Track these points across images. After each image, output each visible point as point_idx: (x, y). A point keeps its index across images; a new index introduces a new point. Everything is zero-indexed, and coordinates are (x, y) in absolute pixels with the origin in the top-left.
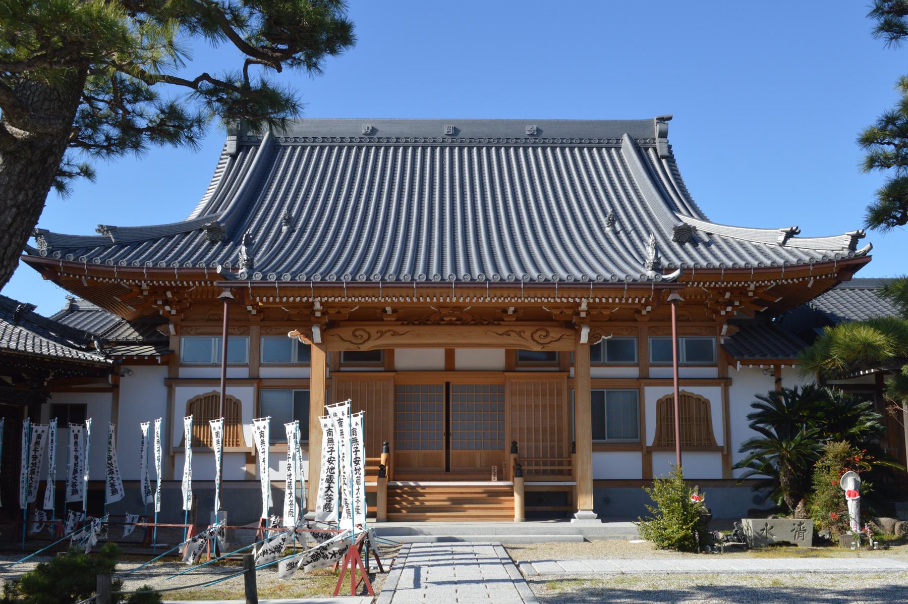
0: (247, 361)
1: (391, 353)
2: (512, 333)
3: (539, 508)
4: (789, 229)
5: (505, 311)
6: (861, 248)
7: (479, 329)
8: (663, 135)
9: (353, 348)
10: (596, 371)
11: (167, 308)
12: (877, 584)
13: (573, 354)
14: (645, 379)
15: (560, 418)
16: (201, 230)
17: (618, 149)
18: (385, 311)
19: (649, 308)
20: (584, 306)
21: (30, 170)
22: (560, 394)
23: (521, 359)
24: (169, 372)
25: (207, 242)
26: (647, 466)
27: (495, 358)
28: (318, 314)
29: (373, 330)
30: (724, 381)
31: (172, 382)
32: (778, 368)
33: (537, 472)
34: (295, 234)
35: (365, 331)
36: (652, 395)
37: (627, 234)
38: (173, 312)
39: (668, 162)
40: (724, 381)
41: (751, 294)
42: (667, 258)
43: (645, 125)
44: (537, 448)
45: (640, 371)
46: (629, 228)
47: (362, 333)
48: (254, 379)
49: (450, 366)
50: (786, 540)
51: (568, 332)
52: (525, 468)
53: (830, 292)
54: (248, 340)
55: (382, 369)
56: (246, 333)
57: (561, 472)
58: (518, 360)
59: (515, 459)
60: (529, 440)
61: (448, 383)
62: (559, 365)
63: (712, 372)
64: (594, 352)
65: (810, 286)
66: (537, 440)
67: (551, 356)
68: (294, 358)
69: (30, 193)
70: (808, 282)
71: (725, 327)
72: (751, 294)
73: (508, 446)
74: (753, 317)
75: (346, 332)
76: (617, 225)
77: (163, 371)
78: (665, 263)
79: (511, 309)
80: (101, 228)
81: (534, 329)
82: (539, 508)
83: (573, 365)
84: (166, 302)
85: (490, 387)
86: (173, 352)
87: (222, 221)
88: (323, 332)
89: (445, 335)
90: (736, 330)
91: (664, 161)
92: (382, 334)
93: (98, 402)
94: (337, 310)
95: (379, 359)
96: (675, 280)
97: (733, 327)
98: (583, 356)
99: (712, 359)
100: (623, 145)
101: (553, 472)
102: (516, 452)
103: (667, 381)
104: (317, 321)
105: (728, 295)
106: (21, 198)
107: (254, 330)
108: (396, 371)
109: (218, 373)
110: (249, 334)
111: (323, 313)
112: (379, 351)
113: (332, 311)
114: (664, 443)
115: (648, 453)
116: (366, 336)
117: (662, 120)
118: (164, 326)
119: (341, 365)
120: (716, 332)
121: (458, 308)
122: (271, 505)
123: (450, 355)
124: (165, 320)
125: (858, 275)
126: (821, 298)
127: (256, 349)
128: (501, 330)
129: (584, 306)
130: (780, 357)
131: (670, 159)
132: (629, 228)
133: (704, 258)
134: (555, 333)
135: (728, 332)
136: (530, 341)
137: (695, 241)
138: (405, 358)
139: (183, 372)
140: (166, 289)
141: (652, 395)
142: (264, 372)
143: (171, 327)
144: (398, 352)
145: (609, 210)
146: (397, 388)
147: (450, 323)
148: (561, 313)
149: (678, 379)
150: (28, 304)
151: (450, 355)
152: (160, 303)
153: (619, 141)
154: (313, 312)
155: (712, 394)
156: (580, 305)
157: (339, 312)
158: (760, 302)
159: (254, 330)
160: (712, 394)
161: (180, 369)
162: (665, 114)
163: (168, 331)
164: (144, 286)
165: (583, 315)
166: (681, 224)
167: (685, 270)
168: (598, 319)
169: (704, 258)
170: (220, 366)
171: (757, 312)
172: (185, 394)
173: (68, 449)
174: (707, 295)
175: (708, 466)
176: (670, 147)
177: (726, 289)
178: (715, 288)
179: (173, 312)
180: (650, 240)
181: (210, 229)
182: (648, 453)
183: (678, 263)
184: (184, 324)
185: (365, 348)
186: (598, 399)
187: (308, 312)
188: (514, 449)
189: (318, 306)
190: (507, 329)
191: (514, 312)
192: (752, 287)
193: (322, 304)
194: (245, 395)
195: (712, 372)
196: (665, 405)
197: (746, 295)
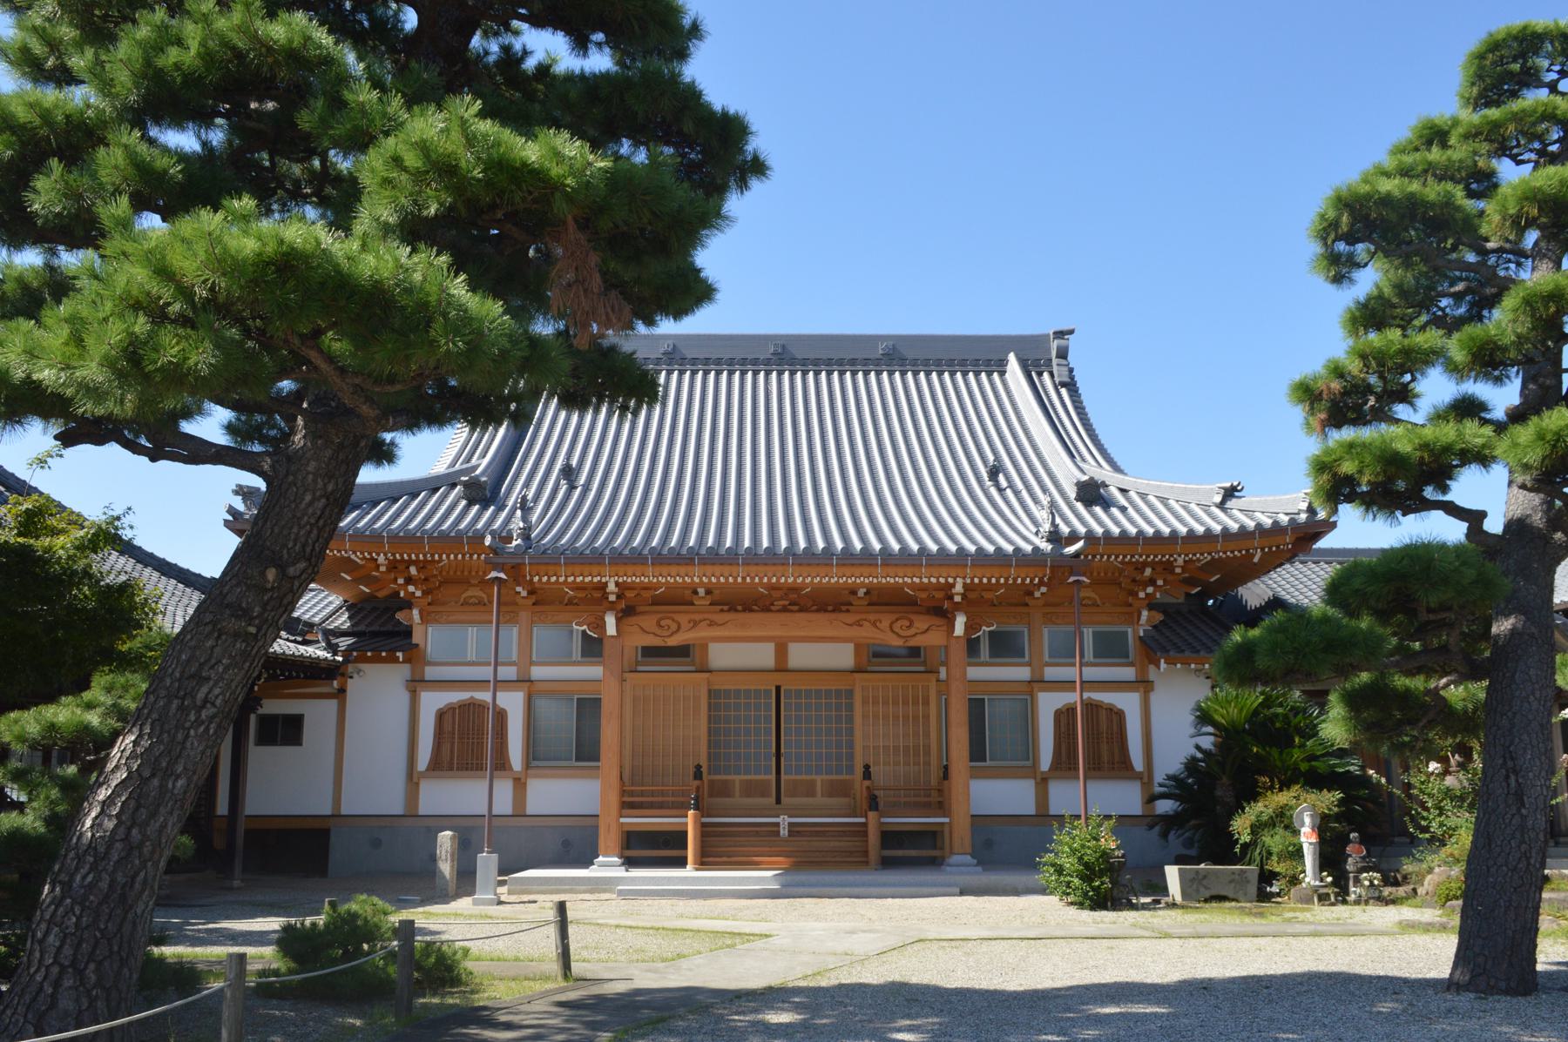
0: (515, 658)
1: (705, 647)
3: (900, 853)
4: (1228, 485)
5: (854, 592)
8: (1063, 354)
9: (657, 642)
10: (975, 673)
11: (411, 588)
12: (1227, 904)
14: (1038, 683)
15: (927, 734)
16: (454, 486)
17: (1002, 373)
18: (695, 592)
19: (1043, 589)
20: (959, 588)
21: (341, 456)
22: (926, 702)
23: (876, 655)
25: (464, 502)
26: (1042, 798)
27: (841, 655)
28: (612, 598)
29: (683, 619)
30: (1143, 685)
31: (416, 684)
34: (577, 492)
36: (1048, 704)
37: (1017, 493)
38: (418, 594)
39: (1069, 391)
40: (1143, 685)
41: (1178, 570)
42: (1067, 522)
43: (1039, 341)
45: (1033, 671)
46: (1020, 485)
48: (524, 681)
49: (781, 667)
50: (1223, 893)
53: (1287, 566)
54: (515, 630)
56: (513, 620)
58: (873, 658)
62: (924, 663)
63: (1128, 673)
64: (972, 646)
65: (1256, 560)
67: (915, 652)
69: (341, 480)
70: (1253, 555)
71: (1145, 613)
72: (1178, 570)
73: (859, 770)
74: (1181, 600)
75: (648, 622)
76: (1001, 478)
78: (1065, 530)
79: (861, 592)
81: (894, 617)
82: (900, 853)
84: (409, 580)
85: (834, 693)
87: (483, 473)
88: (618, 620)
89: (775, 625)
90: (1159, 617)
91: (1064, 391)
92: (695, 624)
93: (317, 714)
96: (1077, 555)
97: (1154, 613)
98: (958, 653)
100: (1009, 368)
103: (1067, 685)
104: (612, 607)
105: (1148, 572)
106: (330, 487)
107: (524, 616)
109: (486, 672)
111: (619, 597)
114: (1064, 763)
115: (1043, 782)
116: (674, 627)
117: (1060, 334)
118: (406, 612)
119: (637, 663)
121: (794, 589)
123: (781, 651)
124: (408, 604)
125: (1323, 543)
126: (1273, 575)
128: (850, 618)
129: (959, 588)
131: (1071, 385)
132: (1020, 485)
133: (1117, 523)
134: (921, 623)
136: (887, 632)
137: (1107, 504)
138: (724, 655)
139: (431, 673)
140: (410, 562)
141: (1048, 704)
142: (538, 672)
143: (415, 612)
144: (714, 649)
145: (991, 457)
146: (712, 694)
147: (784, 610)
149: (1082, 682)
151: (781, 651)
154: (605, 596)
156: (953, 585)
158: (1190, 582)
159: (524, 616)
160: (1128, 702)
162: (1065, 327)
163: (411, 618)
164: (381, 559)
165: (958, 599)
166: (1085, 478)
167: (1090, 537)
168: (976, 602)
169: (1117, 523)
170: (488, 664)
171: (1188, 595)
173: (51, 698)
174: (1121, 571)
175: (1125, 798)
176: (1071, 370)
177: (1145, 564)
178: (1130, 562)
180: (1044, 500)
181: (466, 485)
182: (1043, 782)
183: (1082, 530)
184: (431, 608)
185: (673, 641)
186: (976, 709)
187: (597, 595)
189: (612, 587)
190: (858, 617)
192: (1180, 561)
193: (617, 584)
195: (1128, 673)
196: (1064, 717)
197: (1172, 572)
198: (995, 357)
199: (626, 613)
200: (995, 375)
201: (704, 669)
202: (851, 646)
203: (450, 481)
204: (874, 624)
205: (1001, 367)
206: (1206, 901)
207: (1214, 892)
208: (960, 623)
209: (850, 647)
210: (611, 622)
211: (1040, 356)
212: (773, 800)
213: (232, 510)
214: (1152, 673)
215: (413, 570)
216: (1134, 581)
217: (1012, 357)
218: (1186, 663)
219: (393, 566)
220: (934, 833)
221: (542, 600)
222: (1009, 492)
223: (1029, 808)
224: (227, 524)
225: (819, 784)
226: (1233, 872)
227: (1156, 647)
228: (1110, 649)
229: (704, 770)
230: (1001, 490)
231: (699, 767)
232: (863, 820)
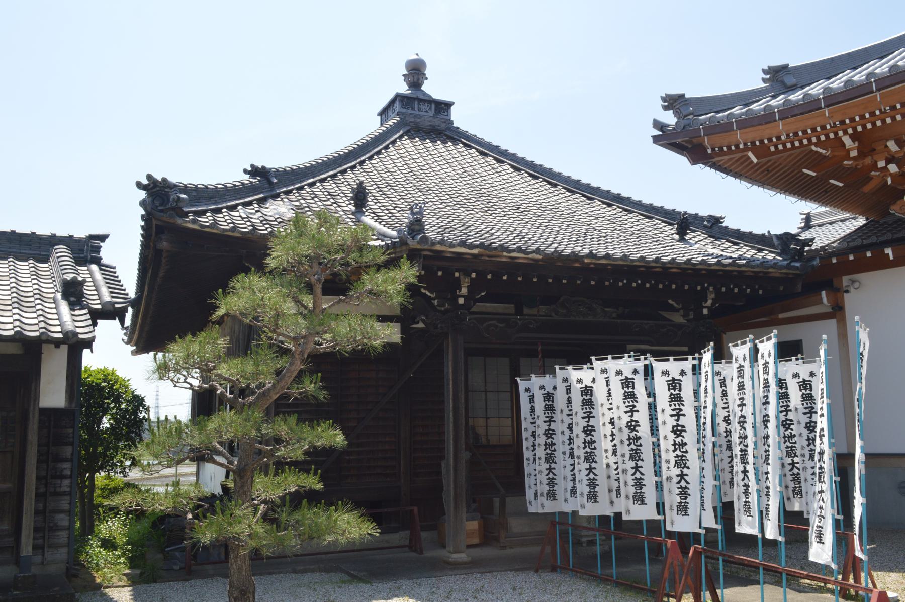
80: (384, 113)
152: (881, 164)
213: (657, 124)
215: (892, 146)
224: (656, 140)
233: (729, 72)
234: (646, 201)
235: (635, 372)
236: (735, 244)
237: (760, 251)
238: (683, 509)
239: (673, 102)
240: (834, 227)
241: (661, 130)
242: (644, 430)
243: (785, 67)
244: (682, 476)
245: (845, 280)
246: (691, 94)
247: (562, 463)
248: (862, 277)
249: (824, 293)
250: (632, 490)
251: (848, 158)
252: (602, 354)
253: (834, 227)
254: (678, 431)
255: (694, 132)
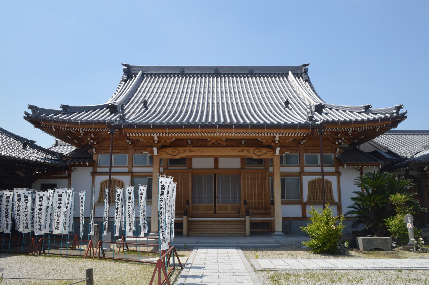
0: (127, 165)
2: (245, 151)
3: (257, 230)
6: (401, 111)
7: (230, 149)
9: (172, 157)
11: (92, 141)
13: (272, 160)
14: (302, 173)
17: (287, 78)
20: (277, 138)
24: (93, 169)
25: (110, 113)
27: (236, 164)
28: (156, 142)
29: (181, 149)
30: (338, 173)
31: (94, 174)
32: (361, 168)
33: (255, 214)
35: (178, 150)
38: (95, 143)
39: (308, 82)
40: (338, 173)
41: (350, 135)
44: (255, 203)
47: (176, 150)
48: (131, 173)
51: (270, 150)
52: (250, 212)
55: (186, 168)
57: (266, 214)
59: (246, 208)
60: (252, 199)
61: (216, 173)
62: (264, 166)
63: (332, 169)
65: (377, 130)
66: (255, 199)
68: (148, 163)
71: (338, 149)
72: (350, 135)
76: (289, 105)
77: (90, 169)
82: (257, 230)
83: (272, 166)
85: (234, 174)
86: (95, 161)
92: (185, 151)
94: (165, 140)
95: (185, 164)
97: (341, 150)
98: (277, 161)
99: (332, 164)
100: (289, 76)
101: (262, 214)
102: (246, 205)
105: (339, 135)
107: (131, 151)
108: (193, 169)
110: (128, 153)
111: (159, 142)
112: (185, 158)
113: (163, 141)
114: (312, 201)
115: (304, 206)
116: (178, 152)
119: (168, 166)
120: (334, 151)
122: (71, 230)
124: (92, 146)
127: (131, 160)
129: (277, 138)
130: (364, 162)
134: (264, 150)
135: (339, 152)
136: (252, 153)
138: (197, 163)
139: (99, 170)
141: (306, 180)
142: (135, 170)
143: (94, 150)
144: (194, 160)
148: (267, 141)
150: (32, 141)
152: (89, 139)
153: (287, 74)
155: (333, 179)
156: (275, 137)
157: (166, 141)
159: (131, 151)
160: (333, 179)
161: (98, 168)
172: (100, 179)
176: (309, 77)
179: (95, 143)
182: (304, 206)
185: (178, 157)
187: (151, 141)
188: (245, 203)
189: (156, 138)
191: (245, 143)
193: (158, 137)
194: (126, 179)
195: (332, 169)
196: (312, 184)
197: (348, 135)
198: (285, 73)
199: (162, 147)
200: (285, 78)
201: (190, 168)
202: (239, 159)
203: (107, 106)
204: (248, 151)
205: (286, 75)
206: (372, 250)
207: (375, 247)
208: (278, 150)
209: (239, 160)
210: (155, 150)
211: (301, 72)
212: (214, 212)
213: (26, 113)
214: (341, 169)
215: (92, 135)
216: (334, 138)
217: (290, 73)
218: (353, 166)
219: (86, 133)
220: (268, 223)
221: (138, 145)
222: (292, 109)
223: (300, 215)
224: (25, 118)
225: (229, 206)
226: (382, 239)
227: (339, 162)
228: (325, 162)
229: (190, 202)
230: (291, 110)
231: (188, 201)
232: (244, 219)
233: (51, 103)
234: (9, 130)
235: (29, 193)
236: (39, 151)
237: (47, 155)
238: (57, 228)
239: (30, 107)
240: (67, 149)
241: (27, 115)
242: (29, 210)
243: (68, 106)
244: (40, 221)
245: (73, 168)
246: (39, 106)
247: (23, 219)
248: (78, 168)
249: (66, 171)
250: (6, 226)
251: (80, 135)
252: (17, 188)
253: (67, 149)
254: (40, 210)
255: (38, 118)
